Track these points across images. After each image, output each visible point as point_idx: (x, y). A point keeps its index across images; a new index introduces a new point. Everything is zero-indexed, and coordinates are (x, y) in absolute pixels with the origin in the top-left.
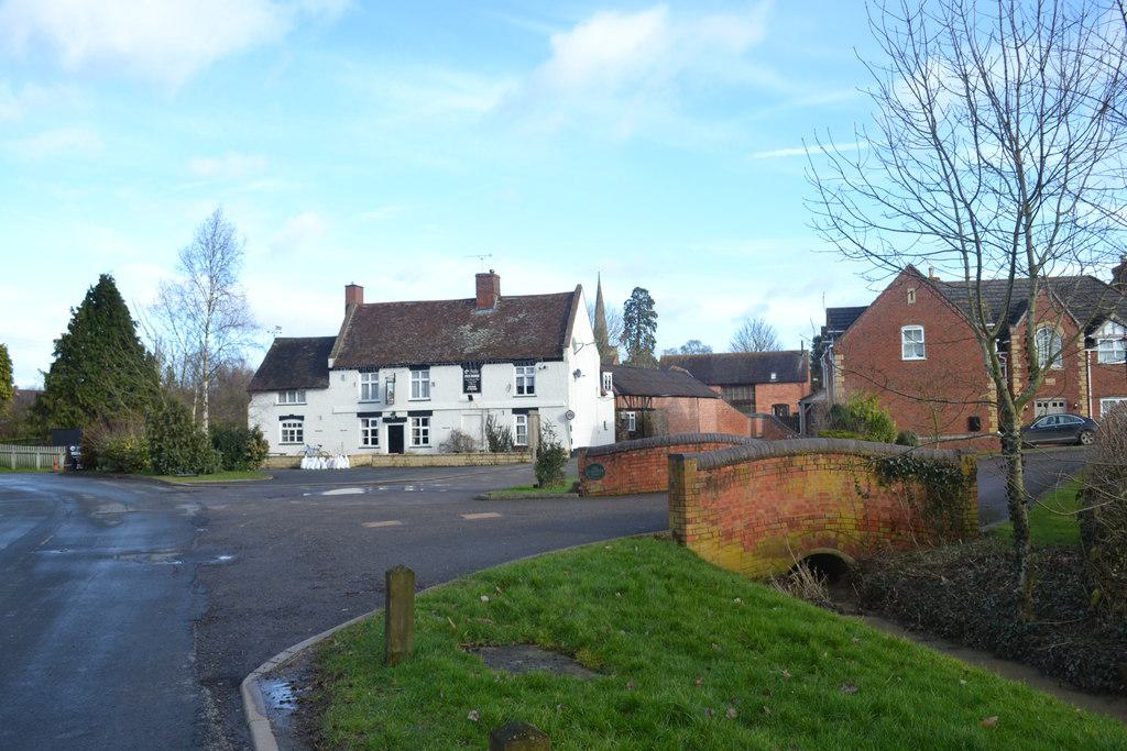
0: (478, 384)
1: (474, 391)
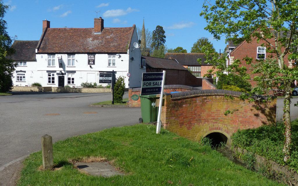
0: (94, 61)
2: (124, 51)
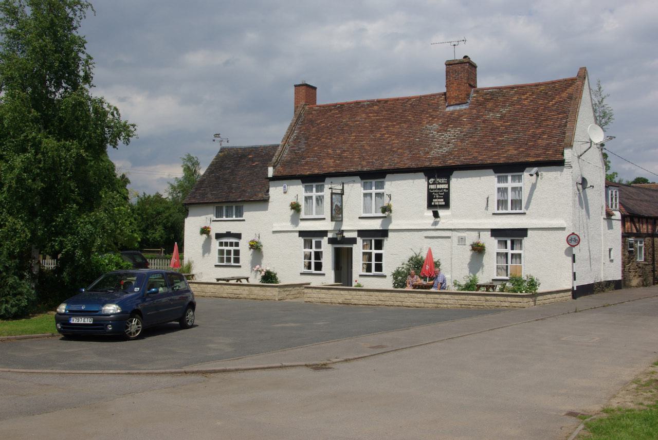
0: (446, 196)
1: (441, 207)
2: (551, 155)
